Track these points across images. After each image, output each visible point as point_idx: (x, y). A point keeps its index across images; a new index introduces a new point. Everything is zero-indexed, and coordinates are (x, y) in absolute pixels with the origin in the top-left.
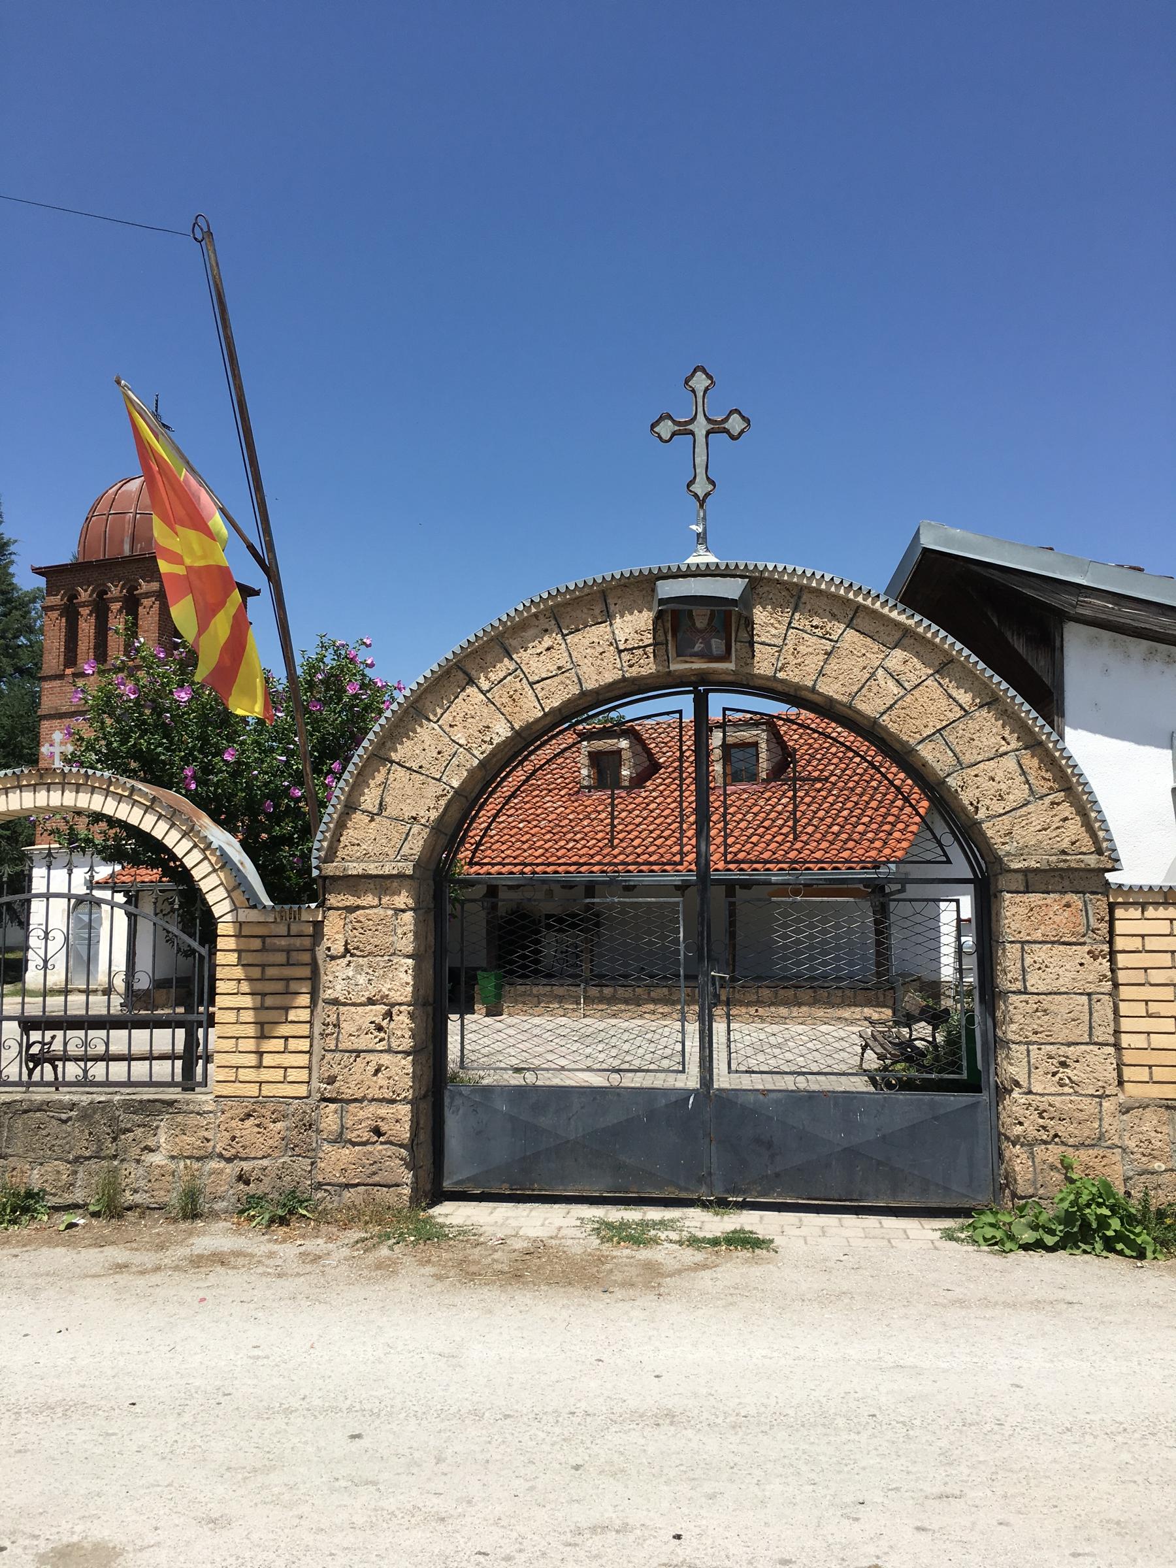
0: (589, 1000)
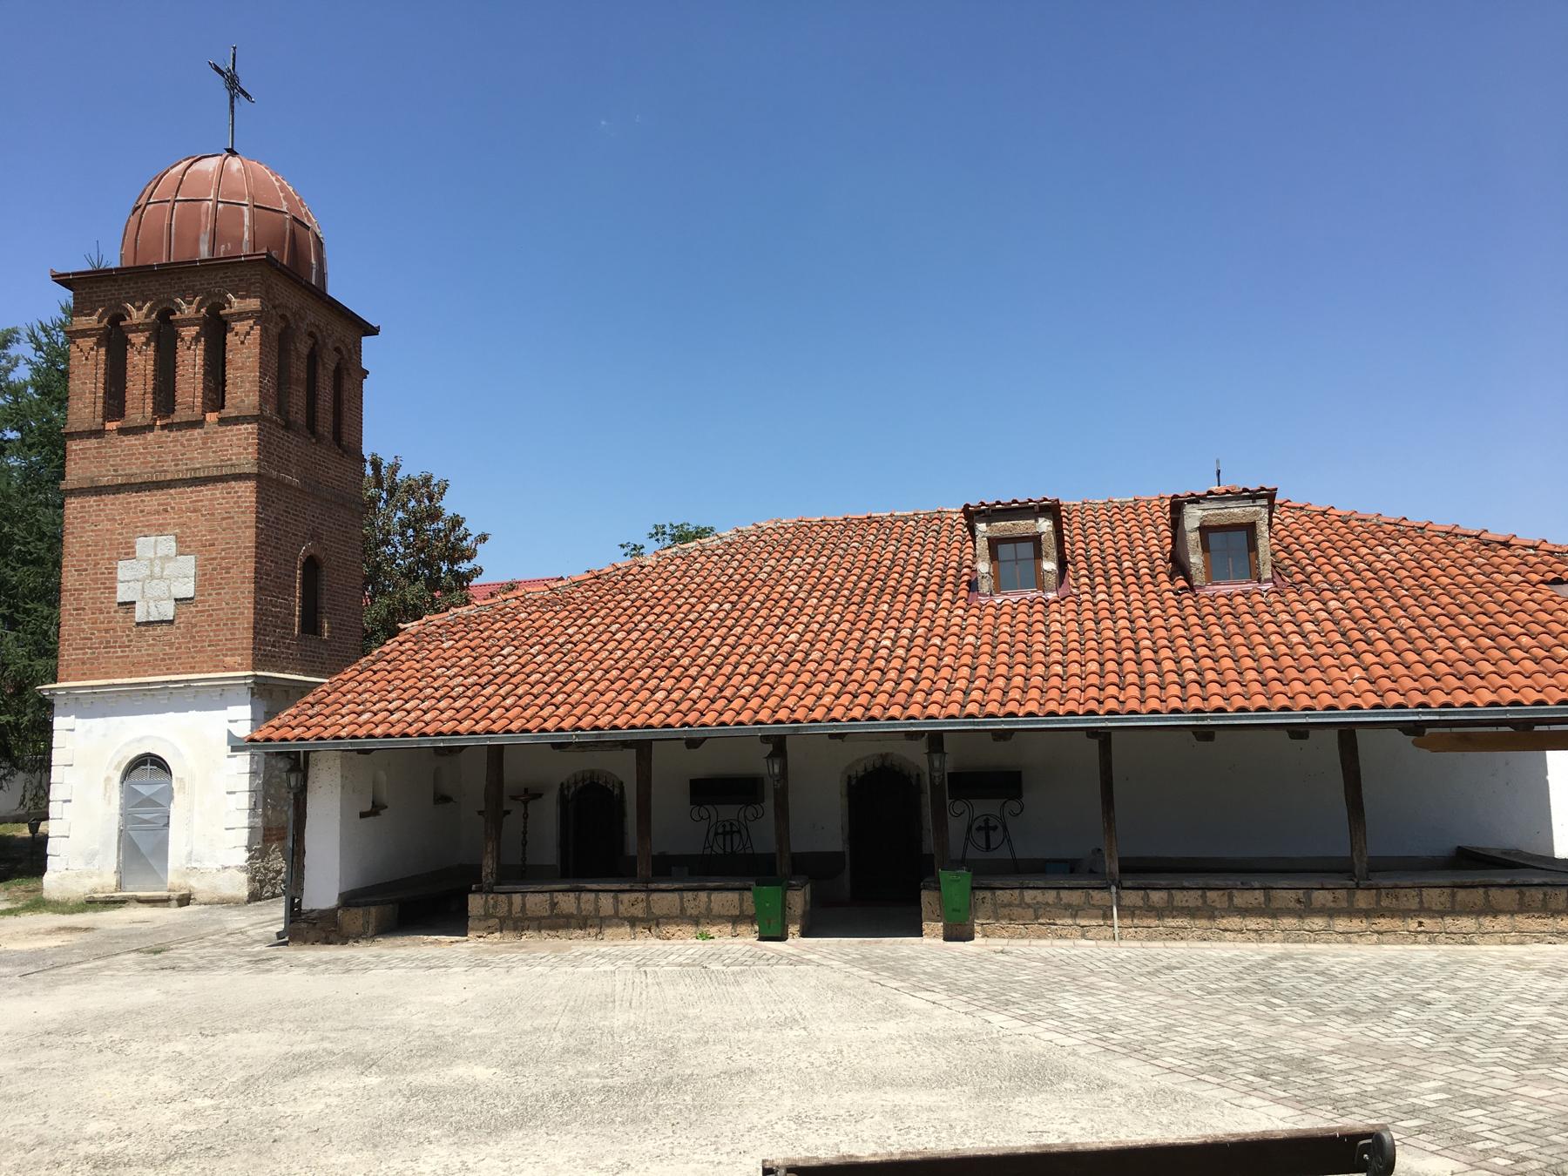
0: (1127, 912)
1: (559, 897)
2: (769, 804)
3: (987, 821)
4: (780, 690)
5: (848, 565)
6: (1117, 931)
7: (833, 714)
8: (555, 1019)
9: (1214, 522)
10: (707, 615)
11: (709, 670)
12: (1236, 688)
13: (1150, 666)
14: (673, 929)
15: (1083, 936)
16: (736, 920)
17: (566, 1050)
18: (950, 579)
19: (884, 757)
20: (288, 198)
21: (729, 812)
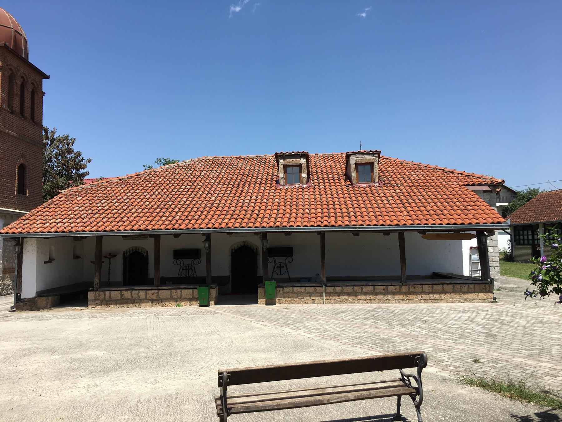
0: (328, 294)
1: (124, 292)
2: (203, 259)
3: (280, 264)
4: (209, 217)
5: (232, 174)
6: (324, 301)
7: (228, 226)
8: (125, 335)
9: (360, 162)
10: (181, 190)
11: (182, 210)
12: (366, 218)
13: (338, 210)
14: (167, 303)
15: (313, 303)
16: (191, 300)
17: (131, 345)
18: (269, 179)
19: (244, 242)
20: (13, 22)
21: (187, 262)
